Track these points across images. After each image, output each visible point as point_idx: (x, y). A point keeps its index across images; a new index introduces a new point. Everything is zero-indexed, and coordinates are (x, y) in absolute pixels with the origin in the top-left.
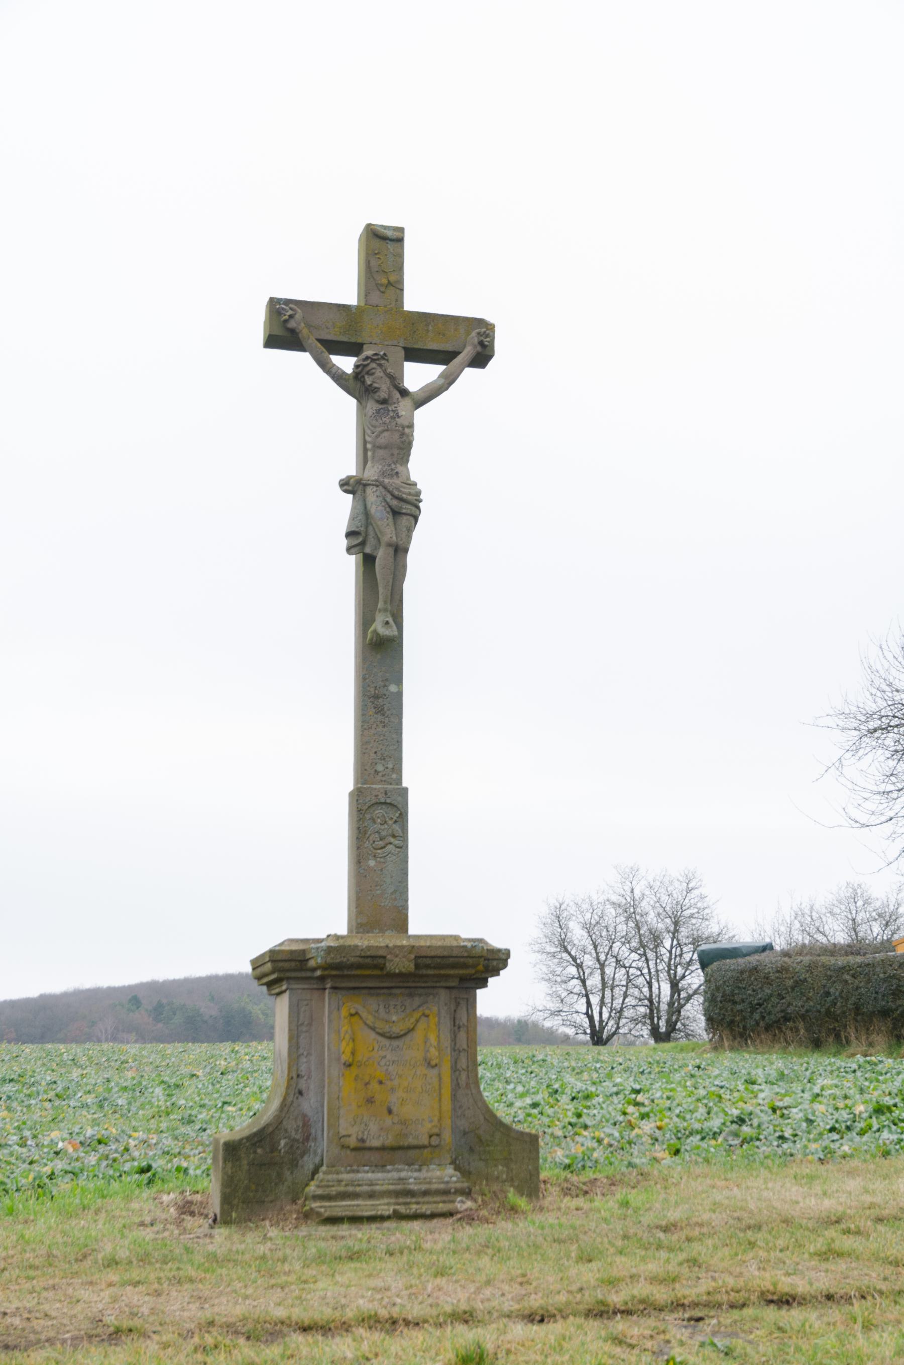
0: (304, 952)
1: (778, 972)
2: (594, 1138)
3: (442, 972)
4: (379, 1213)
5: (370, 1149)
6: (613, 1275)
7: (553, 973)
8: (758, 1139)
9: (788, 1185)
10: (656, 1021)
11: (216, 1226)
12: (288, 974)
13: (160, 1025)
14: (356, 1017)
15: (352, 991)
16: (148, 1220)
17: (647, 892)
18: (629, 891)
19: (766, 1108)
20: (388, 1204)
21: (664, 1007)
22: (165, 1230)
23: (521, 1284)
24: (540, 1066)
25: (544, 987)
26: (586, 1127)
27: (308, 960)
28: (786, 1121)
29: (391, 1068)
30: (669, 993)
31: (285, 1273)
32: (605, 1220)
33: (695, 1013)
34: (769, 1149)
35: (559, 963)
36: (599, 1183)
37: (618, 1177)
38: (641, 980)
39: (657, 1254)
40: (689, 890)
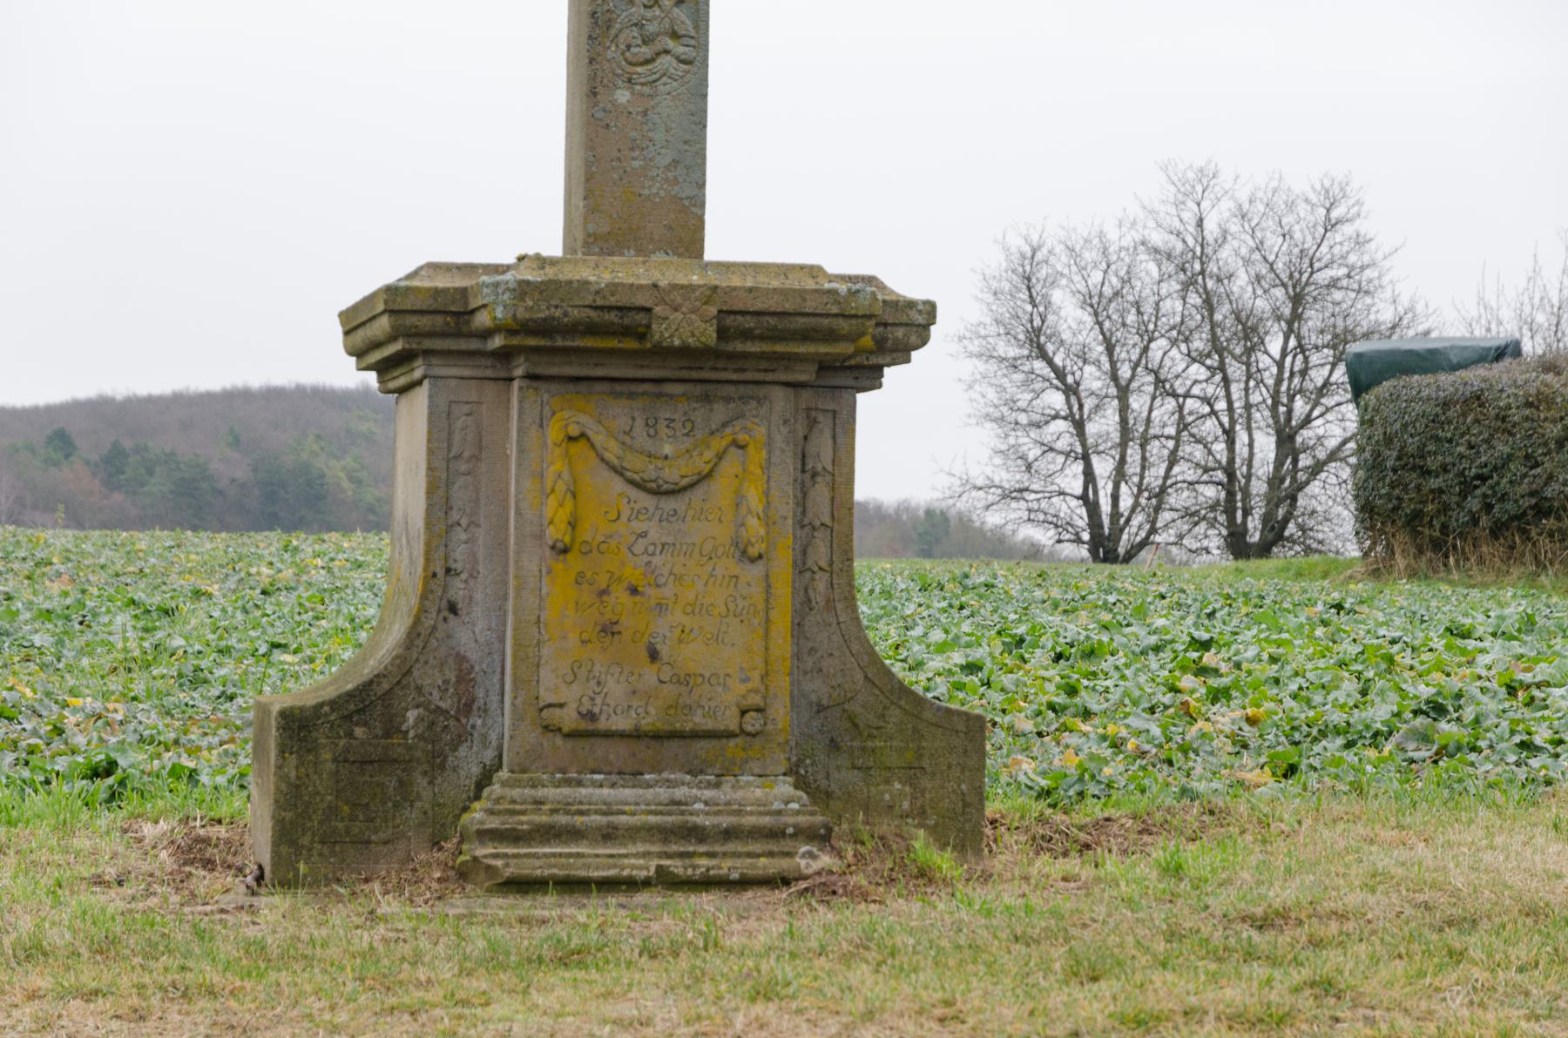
0: (464, 292)
1: (1529, 405)
2: (1104, 738)
3: (780, 348)
4: (625, 873)
5: (608, 735)
6: (1147, 1008)
7: (1011, 403)
8: (1474, 749)
9: (1540, 841)
10: (1239, 520)
11: (263, 890)
12: (428, 344)
13: (118, 497)
14: (582, 443)
15: (571, 386)
16: (110, 872)
17: (1234, 227)
18: (1193, 222)
19: (1495, 685)
20: (645, 855)
21: (1259, 487)
22: (149, 894)
23: (942, 1020)
24: (981, 597)
25: (989, 435)
26: (1087, 714)
27: (473, 311)
28: (1539, 714)
29: (657, 560)
30: (1272, 456)
31: (419, 985)
32: (1129, 902)
33: (1331, 504)
34: (1499, 769)
35: (1026, 384)
36: (1115, 829)
37: (1159, 817)
38: (1209, 427)
39: (1245, 970)
40: (1330, 226)
